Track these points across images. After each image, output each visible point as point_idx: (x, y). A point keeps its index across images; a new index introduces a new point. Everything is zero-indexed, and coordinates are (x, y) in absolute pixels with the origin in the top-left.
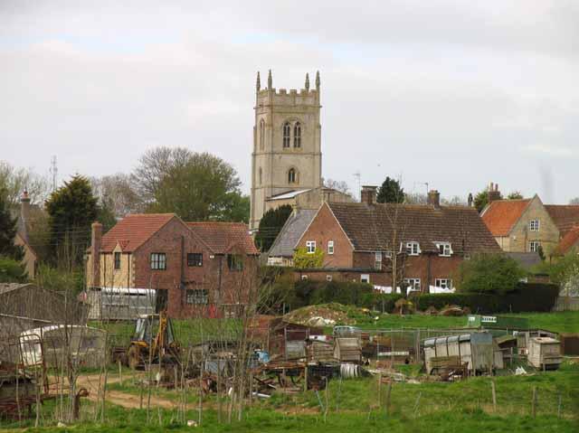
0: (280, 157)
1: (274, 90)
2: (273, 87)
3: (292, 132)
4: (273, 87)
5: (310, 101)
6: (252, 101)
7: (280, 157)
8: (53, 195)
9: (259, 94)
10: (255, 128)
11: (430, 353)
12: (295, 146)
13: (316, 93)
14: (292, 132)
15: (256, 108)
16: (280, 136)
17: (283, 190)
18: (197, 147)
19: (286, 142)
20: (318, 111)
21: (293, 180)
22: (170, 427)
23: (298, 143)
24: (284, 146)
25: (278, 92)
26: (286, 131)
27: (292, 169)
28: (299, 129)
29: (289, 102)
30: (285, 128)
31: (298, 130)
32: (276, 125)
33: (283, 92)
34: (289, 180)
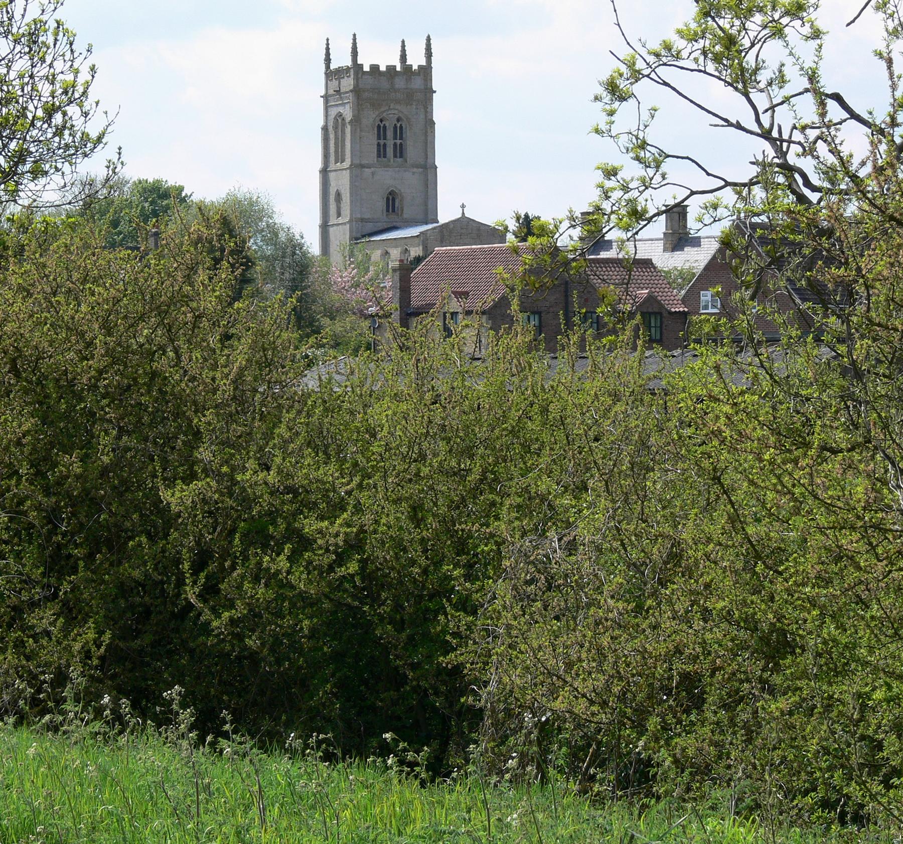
0: (373, 174)
1: (361, 66)
2: (359, 62)
3: (390, 134)
4: (359, 62)
5: (417, 83)
6: (319, 86)
7: (373, 174)
8: (722, 232)
9: (332, 74)
10: (325, 129)
11: (697, 368)
12: (395, 156)
13: (426, 71)
14: (390, 134)
15: (326, 98)
16: (371, 139)
17: (380, 226)
18: (150, 177)
19: (381, 151)
20: (431, 100)
21: (393, 211)
22: (4, 835)
23: (400, 151)
24: (379, 156)
25: (366, 68)
26: (381, 131)
27: (392, 193)
28: (401, 127)
29: (384, 84)
30: (379, 126)
31: (399, 132)
32: (365, 121)
33: (375, 68)
34: (388, 211)
